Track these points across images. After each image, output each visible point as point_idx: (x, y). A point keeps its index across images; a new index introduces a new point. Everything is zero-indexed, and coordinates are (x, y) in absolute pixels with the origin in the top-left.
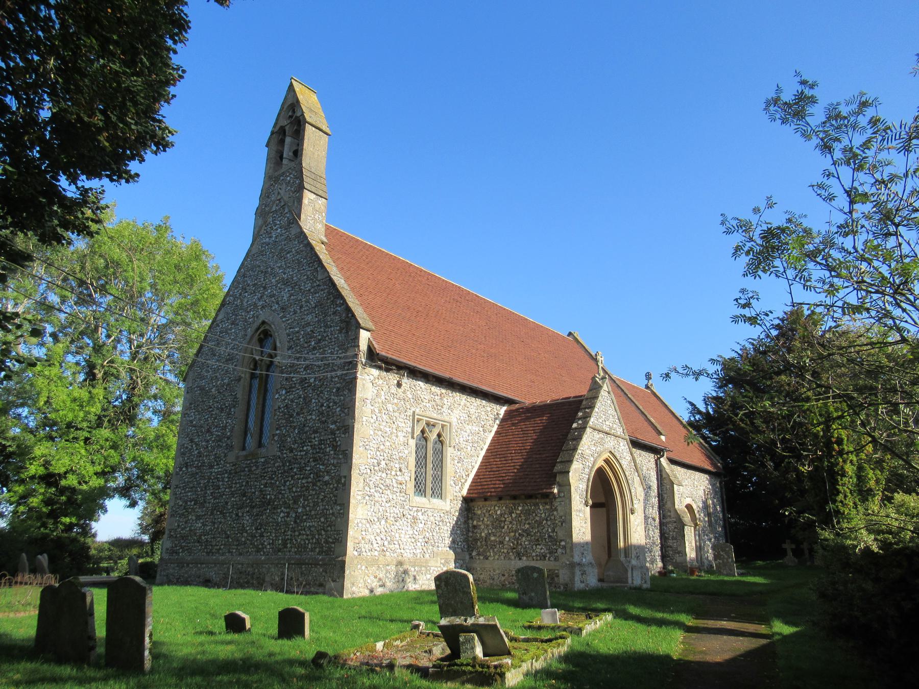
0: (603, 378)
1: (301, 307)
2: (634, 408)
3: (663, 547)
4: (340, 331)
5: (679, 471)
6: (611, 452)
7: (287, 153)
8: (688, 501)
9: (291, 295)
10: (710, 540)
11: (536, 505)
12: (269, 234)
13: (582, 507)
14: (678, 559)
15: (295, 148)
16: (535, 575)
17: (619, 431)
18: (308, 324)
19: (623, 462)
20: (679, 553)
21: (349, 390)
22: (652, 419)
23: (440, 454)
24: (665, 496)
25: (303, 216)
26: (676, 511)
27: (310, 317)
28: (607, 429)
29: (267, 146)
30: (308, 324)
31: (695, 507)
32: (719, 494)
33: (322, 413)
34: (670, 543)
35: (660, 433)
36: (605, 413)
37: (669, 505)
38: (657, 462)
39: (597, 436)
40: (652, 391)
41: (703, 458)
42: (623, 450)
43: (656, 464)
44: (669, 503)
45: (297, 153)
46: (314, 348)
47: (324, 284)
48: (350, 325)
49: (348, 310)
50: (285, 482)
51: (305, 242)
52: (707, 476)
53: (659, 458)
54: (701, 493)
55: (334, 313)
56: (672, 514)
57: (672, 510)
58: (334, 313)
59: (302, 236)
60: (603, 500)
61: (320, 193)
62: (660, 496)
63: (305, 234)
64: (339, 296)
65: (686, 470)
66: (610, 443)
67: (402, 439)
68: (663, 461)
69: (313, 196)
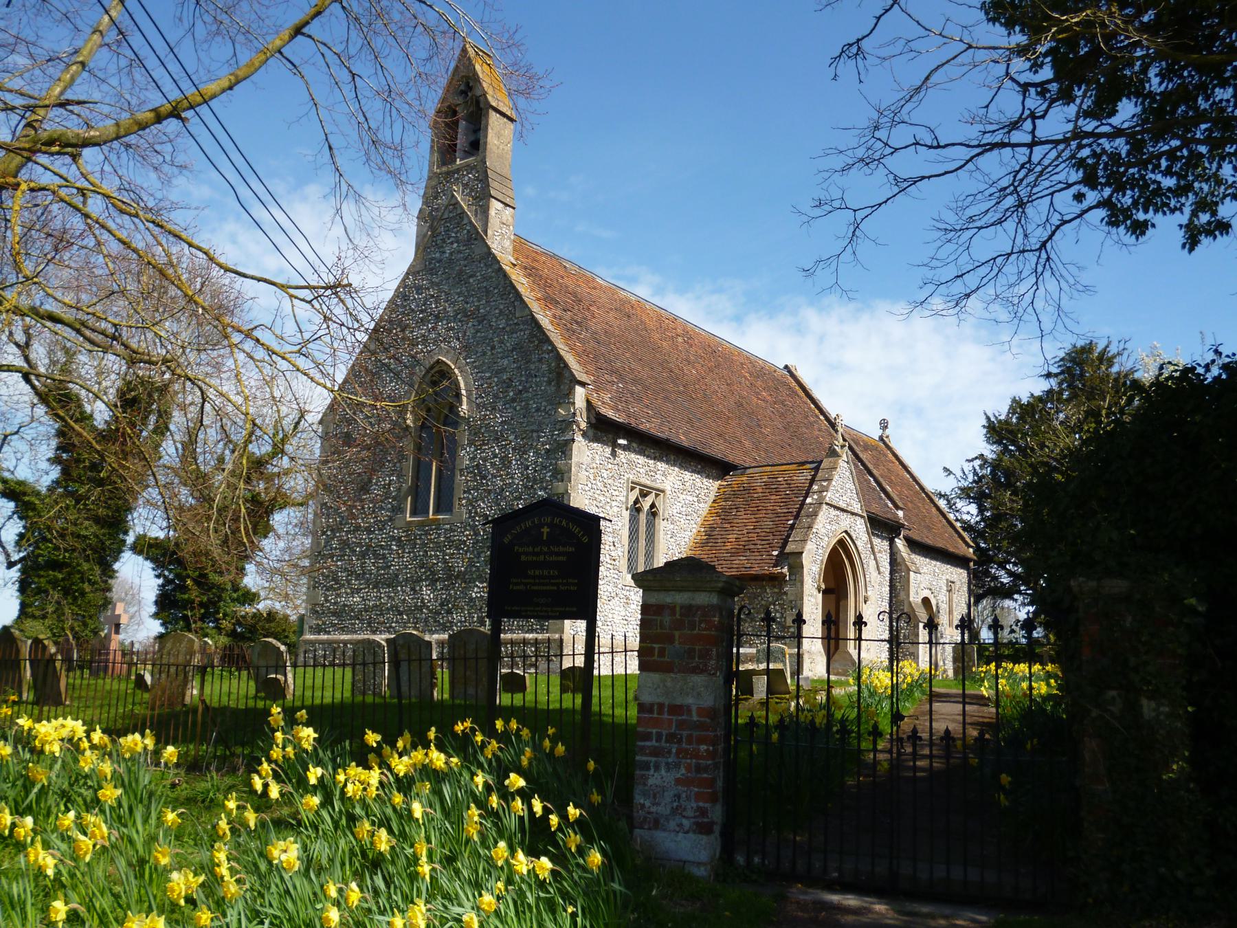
0: (842, 447)
1: (493, 348)
4: (549, 383)
5: (919, 560)
6: (846, 532)
7: (462, 141)
8: (926, 593)
9: (478, 331)
11: (763, 588)
12: (440, 248)
13: (815, 592)
15: (472, 138)
17: (856, 507)
18: (504, 370)
19: (858, 543)
21: (563, 453)
23: (651, 526)
25: (490, 232)
27: (506, 362)
28: (843, 506)
30: (504, 370)
33: (528, 477)
36: (842, 485)
37: (902, 596)
39: (834, 512)
42: (860, 529)
45: (476, 146)
46: (513, 400)
47: (524, 323)
48: (563, 380)
49: (560, 358)
50: (479, 554)
51: (496, 267)
55: (540, 360)
58: (540, 360)
59: (489, 258)
60: (832, 586)
61: (508, 201)
63: (494, 257)
64: (547, 340)
66: (846, 522)
67: (615, 509)
69: (499, 206)
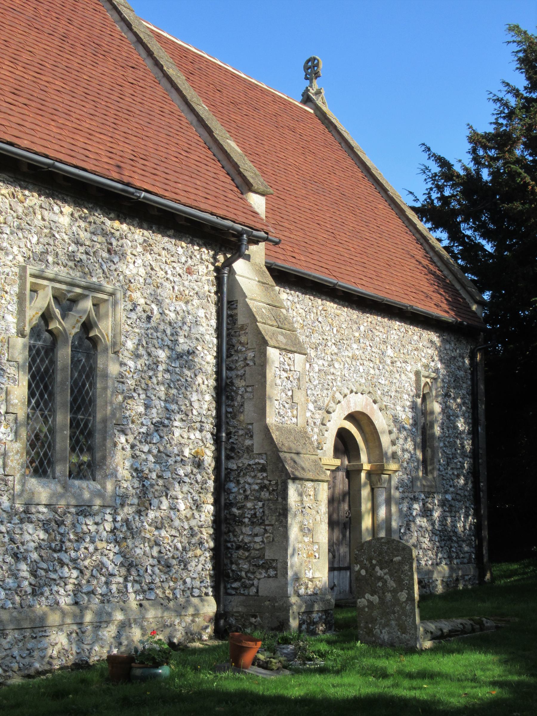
2: (177, 105)
3: (220, 556)
10: (426, 513)
14: (264, 585)
16: (380, 584)
20: (267, 565)
22: (232, 146)
24: (240, 383)
26: (266, 430)
29: (303, 95)
31: (381, 422)
32: (466, 385)
34: (245, 533)
35: (246, 186)
37: (248, 414)
38: (223, 278)
40: (317, 108)
41: (425, 284)
43: (219, 280)
44: (249, 407)
52: (434, 337)
53: (228, 263)
54: (408, 383)
56: (256, 443)
57: (256, 429)
62: (223, 391)
65: (355, 314)
68: (248, 273)
